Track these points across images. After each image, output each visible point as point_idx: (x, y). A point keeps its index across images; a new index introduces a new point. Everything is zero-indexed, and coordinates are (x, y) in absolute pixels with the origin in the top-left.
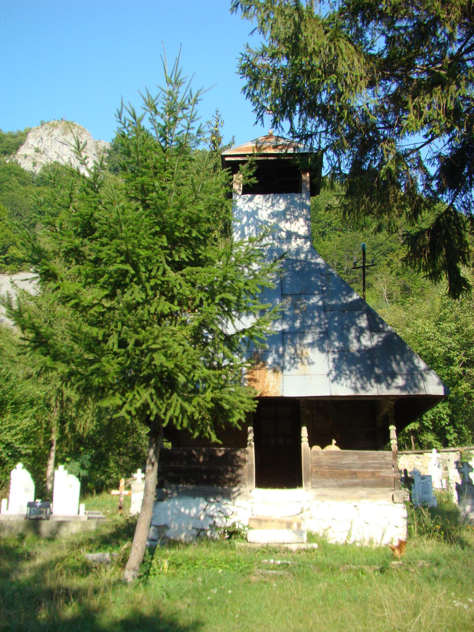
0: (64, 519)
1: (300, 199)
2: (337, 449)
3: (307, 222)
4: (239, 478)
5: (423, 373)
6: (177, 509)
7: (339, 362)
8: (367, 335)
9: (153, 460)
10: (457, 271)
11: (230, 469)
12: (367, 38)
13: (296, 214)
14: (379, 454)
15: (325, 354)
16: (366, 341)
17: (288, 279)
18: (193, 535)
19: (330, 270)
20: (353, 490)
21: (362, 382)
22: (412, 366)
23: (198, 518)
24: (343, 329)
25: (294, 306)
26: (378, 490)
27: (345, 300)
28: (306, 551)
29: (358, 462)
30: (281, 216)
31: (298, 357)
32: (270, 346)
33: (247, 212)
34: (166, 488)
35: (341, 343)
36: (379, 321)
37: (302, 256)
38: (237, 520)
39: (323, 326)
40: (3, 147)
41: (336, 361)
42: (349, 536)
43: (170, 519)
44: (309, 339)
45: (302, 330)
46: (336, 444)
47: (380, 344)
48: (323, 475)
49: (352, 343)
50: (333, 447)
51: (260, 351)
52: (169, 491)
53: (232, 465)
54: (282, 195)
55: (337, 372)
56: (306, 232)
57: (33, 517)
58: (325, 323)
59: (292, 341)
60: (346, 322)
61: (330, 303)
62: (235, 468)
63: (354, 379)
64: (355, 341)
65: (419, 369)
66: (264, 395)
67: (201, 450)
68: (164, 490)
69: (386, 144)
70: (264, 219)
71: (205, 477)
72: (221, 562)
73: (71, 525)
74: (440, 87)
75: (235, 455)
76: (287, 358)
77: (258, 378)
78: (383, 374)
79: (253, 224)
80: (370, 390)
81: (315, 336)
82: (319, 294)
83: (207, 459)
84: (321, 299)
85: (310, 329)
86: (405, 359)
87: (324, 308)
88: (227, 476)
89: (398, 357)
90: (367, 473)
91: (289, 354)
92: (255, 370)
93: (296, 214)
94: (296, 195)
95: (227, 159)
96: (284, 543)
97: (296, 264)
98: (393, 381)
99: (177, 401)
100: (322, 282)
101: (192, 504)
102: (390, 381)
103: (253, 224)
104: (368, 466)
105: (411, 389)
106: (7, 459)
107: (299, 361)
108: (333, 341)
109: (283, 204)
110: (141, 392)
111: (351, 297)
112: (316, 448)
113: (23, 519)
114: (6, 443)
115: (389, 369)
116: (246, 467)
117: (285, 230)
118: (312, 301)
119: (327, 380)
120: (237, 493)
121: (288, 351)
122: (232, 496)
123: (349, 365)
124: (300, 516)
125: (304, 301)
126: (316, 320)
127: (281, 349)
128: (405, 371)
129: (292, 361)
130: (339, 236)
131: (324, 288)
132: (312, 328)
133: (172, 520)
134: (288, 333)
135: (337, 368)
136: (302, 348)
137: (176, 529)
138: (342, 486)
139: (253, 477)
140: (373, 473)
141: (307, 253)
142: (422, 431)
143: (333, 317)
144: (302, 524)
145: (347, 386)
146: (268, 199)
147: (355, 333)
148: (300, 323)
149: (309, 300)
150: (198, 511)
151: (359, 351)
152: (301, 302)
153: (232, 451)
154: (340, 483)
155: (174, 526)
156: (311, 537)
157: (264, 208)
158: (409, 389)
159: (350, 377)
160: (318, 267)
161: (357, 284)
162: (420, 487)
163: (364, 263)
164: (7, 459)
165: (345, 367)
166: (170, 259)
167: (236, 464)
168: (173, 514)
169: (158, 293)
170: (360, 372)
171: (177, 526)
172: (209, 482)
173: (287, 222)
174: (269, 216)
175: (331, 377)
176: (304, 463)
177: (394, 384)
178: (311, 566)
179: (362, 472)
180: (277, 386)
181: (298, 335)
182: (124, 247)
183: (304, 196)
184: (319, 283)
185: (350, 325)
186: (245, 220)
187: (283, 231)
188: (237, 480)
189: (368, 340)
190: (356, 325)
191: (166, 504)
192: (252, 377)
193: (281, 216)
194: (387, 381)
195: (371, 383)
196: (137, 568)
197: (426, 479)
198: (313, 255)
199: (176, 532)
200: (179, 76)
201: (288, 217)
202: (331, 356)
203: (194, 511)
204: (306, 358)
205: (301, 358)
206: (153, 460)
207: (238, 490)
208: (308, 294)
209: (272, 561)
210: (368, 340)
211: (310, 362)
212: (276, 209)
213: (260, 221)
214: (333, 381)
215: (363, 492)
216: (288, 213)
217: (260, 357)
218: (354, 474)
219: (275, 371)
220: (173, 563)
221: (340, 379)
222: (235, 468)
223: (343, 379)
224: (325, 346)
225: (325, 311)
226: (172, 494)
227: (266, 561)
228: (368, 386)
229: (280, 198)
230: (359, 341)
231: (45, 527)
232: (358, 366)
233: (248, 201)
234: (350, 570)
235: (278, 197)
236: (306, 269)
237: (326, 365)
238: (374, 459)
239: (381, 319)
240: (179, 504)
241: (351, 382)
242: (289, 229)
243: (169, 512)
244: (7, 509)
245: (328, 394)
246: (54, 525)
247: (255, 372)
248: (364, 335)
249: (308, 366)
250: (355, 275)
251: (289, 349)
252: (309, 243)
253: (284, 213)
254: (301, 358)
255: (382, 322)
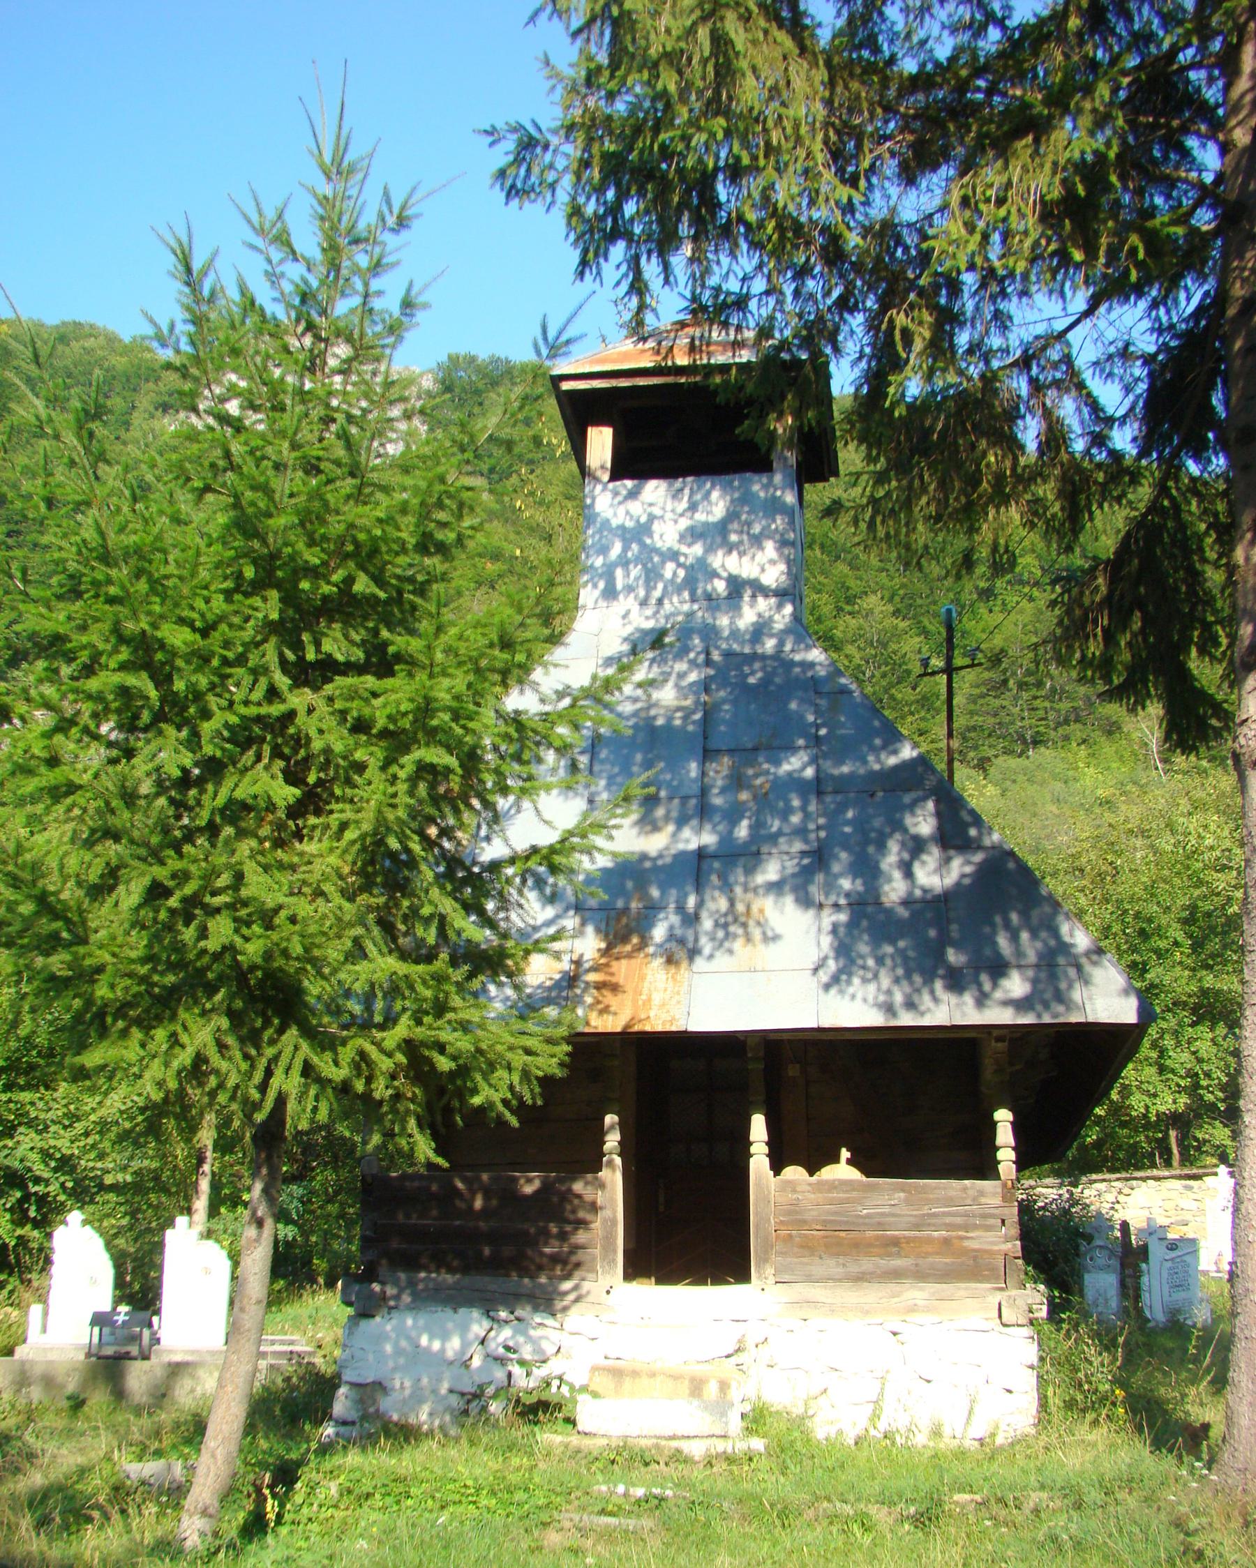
0: (189, 1358)
1: (765, 487)
2: (854, 1174)
3: (786, 551)
4: (580, 1256)
5: (1084, 960)
6: (408, 1338)
7: (849, 933)
8: (932, 857)
9: (260, 1213)
10: (1184, 675)
11: (554, 1230)
12: (893, 24)
13: (757, 529)
14: (965, 1189)
15: (811, 913)
16: (929, 874)
17: (726, 707)
18: (449, 1409)
19: (843, 681)
20: (892, 1287)
21: (908, 989)
22: (1052, 943)
23: (466, 1364)
24: (866, 842)
25: (737, 781)
26: (961, 1289)
27: (878, 761)
28: (730, 1459)
29: (904, 1210)
30: (716, 535)
31: (736, 920)
32: (663, 893)
33: (622, 527)
34: (383, 1283)
35: (859, 882)
36: (968, 818)
37: (770, 645)
38: (557, 1372)
39: (812, 836)
40: (159, 393)
41: (842, 930)
42: (875, 1416)
43: (391, 1364)
44: (771, 871)
45: (754, 848)
46: (849, 1162)
47: (967, 881)
48: (808, 1248)
49: (890, 880)
50: (842, 1171)
51: (634, 905)
52: (391, 1291)
53: (562, 1220)
54: (717, 479)
55: (841, 962)
56: (784, 578)
57: (109, 1351)
58: (819, 828)
59: (723, 877)
60: (877, 823)
61: (836, 772)
62: (568, 1228)
63: (886, 981)
64: (897, 875)
65: (1074, 951)
66: (636, 1028)
67: (479, 1179)
68: (376, 1287)
69: (902, 314)
70: (668, 545)
71: (487, 1251)
72: (478, 1489)
73: (201, 1373)
74: (1030, 138)
75: (570, 1190)
76: (707, 924)
77: (621, 982)
78: (969, 964)
79: (637, 560)
80: (929, 1010)
81: (789, 864)
82: (806, 747)
83: (494, 1202)
84: (814, 760)
85: (775, 844)
86: (1035, 921)
87: (818, 787)
88: (547, 1250)
89: (1014, 917)
90: (930, 1240)
91: (711, 914)
92: (617, 959)
93: (757, 529)
94: (756, 477)
95: (566, 386)
96: (673, 1437)
97: (750, 665)
98: (995, 985)
99: (296, 1048)
100: (817, 713)
101: (450, 1325)
102: (987, 986)
103: (637, 560)
104: (933, 1221)
105: (1046, 1006)
106: (62, 1198)
107: (740, 931)
108: (837, 877)
109: (721, 504)
110: (190, 1024)
111: (895, 752)
112: (794, 1173)
113: (82, 1357)
114: (58, 1155)
115: (988, 952)
116: (597, 1224)
117: (725, 575)
118: (786, 767)
119: (812, 984)
120: (572, 1297)
121: (710, 905)
122: (559, 1305)
123: (876, 942)
124: (734, 1360)
125: (766, 766)
126: (795, 819)
127: (691, 901)
128: (1031, 957)
129: (721, 934)
130: (1031, 599)
131: (823, 732)
132: (782, 840)
133: (395, 1369)
134: (715, 856)
135: (843, 950)
136: (750, 895)
137: (407, 1392)
138: (860, 1278)
139: (615, 1251)
140: (946, 1241)
141: (781, 637)
142: (1198, 1116)
143: (842, 808)
144: (734, 1384)
145: (865, 1000)
146: (681, 490)
147: (899, 853)
148: (750, 827)
149: (777, 763)
150: (465, 1345)
151: (906, 903)
152: (757, 770)
153: (561, 1180)
154: (854, 1269)
155: (401, 1384)
156: (756, 1420)
157: (669, 516)
158: (1039, 1007)
159: (876, 976)
160: (810, 674)
161: (1078, 726)
162: (1165, 1274)
163: (949, 659)
164: (62, 1198)
165: (863, 948)
166: (290, 656)
167: (572, 1217)
168: (399, 1352)
169: (267, 750)
170: (906, 960)
171: (407, 1384)
172: (497, 1266)
173: (730, 552)
174: (682, 538)
175: (824, 976)
176: (756, 1214)
177: (998, 995)
178: (726, 1505)
179: (915, 1239)
180: (674, 1001)
181: (742, 861)
182: (130, 627)
183: (778, 478)
184: (811, 718)
185: (888, 830)
186: (616, 550)
187: (719, 576)
188: (574, 1259)
189: (935, 871)
190: (905, 830)
191: (381, 1324)
192: (608, 978)
193: (716, 535)
194: (979, 985)
195: (932, 992)
196: (211, 1510)
197: (1184, 1249)
198: (799, 640)
199: (404, 1401)
200: (345, 150)
201: (734, 538)
202: (829, 918)
203: (455, 1343)
204: (759, 923)
205: (744, 925)
206: (260, 1213)
207: (576, 1288)
208: (779, 747)
209: (621, 1489)
210: (935, 871)
211: (770, 934)
212: (700, 517)
213: (656, 550)
214: (827, 987)
215: (917, 1293)
216: (735, 526)
217: (633, 924)
218: (893, 1245)
219: (670, 961)
220: (349, 1491)
221: (849, 983)
222: (568, 1228)
223: (856, 981)
224: (813, 889)
225: (820, 793)
226: (397, 1297)
227: (604, 1488)
228: (926, 1000)
229: (713, 487)
230: (908, 874)
231: (138, 1377)
232: (901, 944)
233: (626, 498)
234: (832, 1518)
235: (708, 485)
236: (777, 680)
237: (814, 942)
238: (949, 1202)
239: (972, 812)
240: (415, 1326)
241: (879, 989)
242: (735, 572)
243: (389, 1348)
244: (44, 1330)
245: (812, 1024)
246: (159, 1372)
247: (614, 964)
248: (925, 857)
249: (761, 947)
250: (1073, 699)
251: (713, 899)
252: (788, 609)
253: (722, 528)
254: (744, 925)
255: (977, 820)
